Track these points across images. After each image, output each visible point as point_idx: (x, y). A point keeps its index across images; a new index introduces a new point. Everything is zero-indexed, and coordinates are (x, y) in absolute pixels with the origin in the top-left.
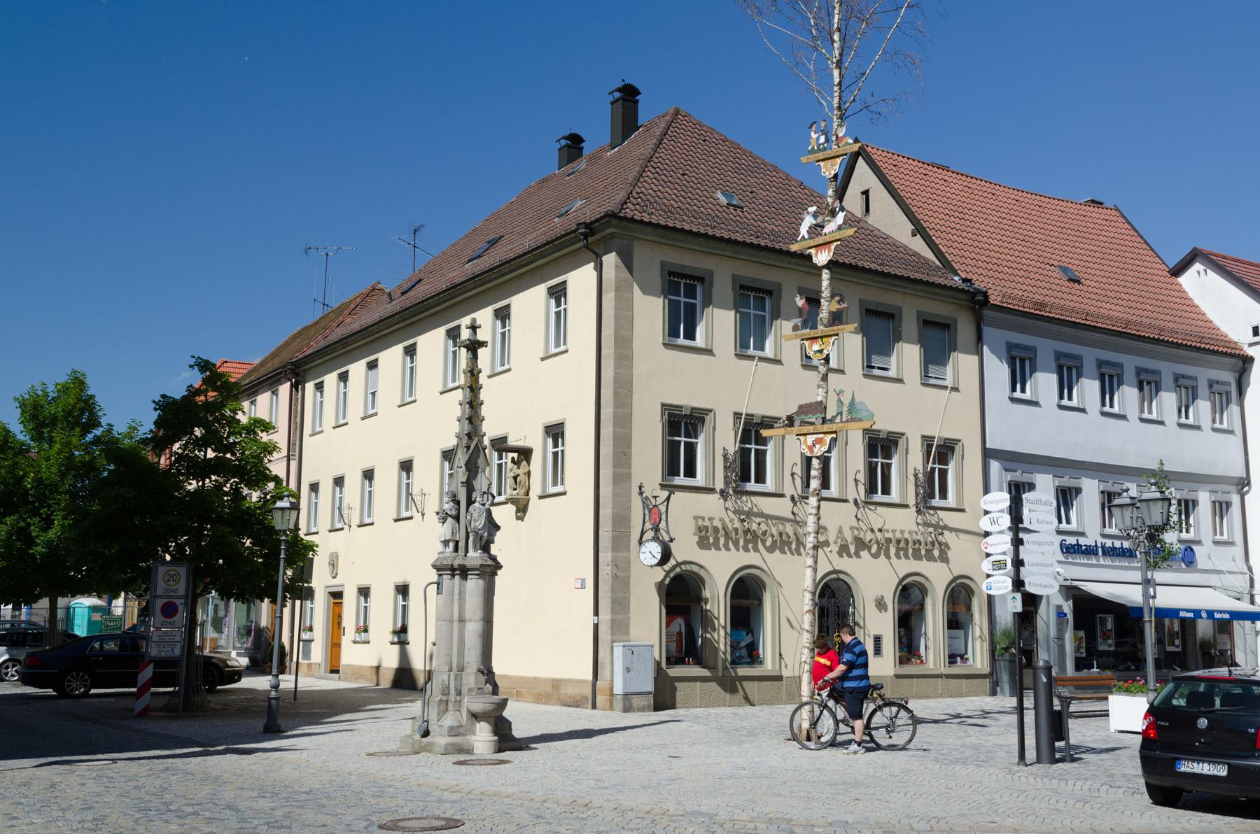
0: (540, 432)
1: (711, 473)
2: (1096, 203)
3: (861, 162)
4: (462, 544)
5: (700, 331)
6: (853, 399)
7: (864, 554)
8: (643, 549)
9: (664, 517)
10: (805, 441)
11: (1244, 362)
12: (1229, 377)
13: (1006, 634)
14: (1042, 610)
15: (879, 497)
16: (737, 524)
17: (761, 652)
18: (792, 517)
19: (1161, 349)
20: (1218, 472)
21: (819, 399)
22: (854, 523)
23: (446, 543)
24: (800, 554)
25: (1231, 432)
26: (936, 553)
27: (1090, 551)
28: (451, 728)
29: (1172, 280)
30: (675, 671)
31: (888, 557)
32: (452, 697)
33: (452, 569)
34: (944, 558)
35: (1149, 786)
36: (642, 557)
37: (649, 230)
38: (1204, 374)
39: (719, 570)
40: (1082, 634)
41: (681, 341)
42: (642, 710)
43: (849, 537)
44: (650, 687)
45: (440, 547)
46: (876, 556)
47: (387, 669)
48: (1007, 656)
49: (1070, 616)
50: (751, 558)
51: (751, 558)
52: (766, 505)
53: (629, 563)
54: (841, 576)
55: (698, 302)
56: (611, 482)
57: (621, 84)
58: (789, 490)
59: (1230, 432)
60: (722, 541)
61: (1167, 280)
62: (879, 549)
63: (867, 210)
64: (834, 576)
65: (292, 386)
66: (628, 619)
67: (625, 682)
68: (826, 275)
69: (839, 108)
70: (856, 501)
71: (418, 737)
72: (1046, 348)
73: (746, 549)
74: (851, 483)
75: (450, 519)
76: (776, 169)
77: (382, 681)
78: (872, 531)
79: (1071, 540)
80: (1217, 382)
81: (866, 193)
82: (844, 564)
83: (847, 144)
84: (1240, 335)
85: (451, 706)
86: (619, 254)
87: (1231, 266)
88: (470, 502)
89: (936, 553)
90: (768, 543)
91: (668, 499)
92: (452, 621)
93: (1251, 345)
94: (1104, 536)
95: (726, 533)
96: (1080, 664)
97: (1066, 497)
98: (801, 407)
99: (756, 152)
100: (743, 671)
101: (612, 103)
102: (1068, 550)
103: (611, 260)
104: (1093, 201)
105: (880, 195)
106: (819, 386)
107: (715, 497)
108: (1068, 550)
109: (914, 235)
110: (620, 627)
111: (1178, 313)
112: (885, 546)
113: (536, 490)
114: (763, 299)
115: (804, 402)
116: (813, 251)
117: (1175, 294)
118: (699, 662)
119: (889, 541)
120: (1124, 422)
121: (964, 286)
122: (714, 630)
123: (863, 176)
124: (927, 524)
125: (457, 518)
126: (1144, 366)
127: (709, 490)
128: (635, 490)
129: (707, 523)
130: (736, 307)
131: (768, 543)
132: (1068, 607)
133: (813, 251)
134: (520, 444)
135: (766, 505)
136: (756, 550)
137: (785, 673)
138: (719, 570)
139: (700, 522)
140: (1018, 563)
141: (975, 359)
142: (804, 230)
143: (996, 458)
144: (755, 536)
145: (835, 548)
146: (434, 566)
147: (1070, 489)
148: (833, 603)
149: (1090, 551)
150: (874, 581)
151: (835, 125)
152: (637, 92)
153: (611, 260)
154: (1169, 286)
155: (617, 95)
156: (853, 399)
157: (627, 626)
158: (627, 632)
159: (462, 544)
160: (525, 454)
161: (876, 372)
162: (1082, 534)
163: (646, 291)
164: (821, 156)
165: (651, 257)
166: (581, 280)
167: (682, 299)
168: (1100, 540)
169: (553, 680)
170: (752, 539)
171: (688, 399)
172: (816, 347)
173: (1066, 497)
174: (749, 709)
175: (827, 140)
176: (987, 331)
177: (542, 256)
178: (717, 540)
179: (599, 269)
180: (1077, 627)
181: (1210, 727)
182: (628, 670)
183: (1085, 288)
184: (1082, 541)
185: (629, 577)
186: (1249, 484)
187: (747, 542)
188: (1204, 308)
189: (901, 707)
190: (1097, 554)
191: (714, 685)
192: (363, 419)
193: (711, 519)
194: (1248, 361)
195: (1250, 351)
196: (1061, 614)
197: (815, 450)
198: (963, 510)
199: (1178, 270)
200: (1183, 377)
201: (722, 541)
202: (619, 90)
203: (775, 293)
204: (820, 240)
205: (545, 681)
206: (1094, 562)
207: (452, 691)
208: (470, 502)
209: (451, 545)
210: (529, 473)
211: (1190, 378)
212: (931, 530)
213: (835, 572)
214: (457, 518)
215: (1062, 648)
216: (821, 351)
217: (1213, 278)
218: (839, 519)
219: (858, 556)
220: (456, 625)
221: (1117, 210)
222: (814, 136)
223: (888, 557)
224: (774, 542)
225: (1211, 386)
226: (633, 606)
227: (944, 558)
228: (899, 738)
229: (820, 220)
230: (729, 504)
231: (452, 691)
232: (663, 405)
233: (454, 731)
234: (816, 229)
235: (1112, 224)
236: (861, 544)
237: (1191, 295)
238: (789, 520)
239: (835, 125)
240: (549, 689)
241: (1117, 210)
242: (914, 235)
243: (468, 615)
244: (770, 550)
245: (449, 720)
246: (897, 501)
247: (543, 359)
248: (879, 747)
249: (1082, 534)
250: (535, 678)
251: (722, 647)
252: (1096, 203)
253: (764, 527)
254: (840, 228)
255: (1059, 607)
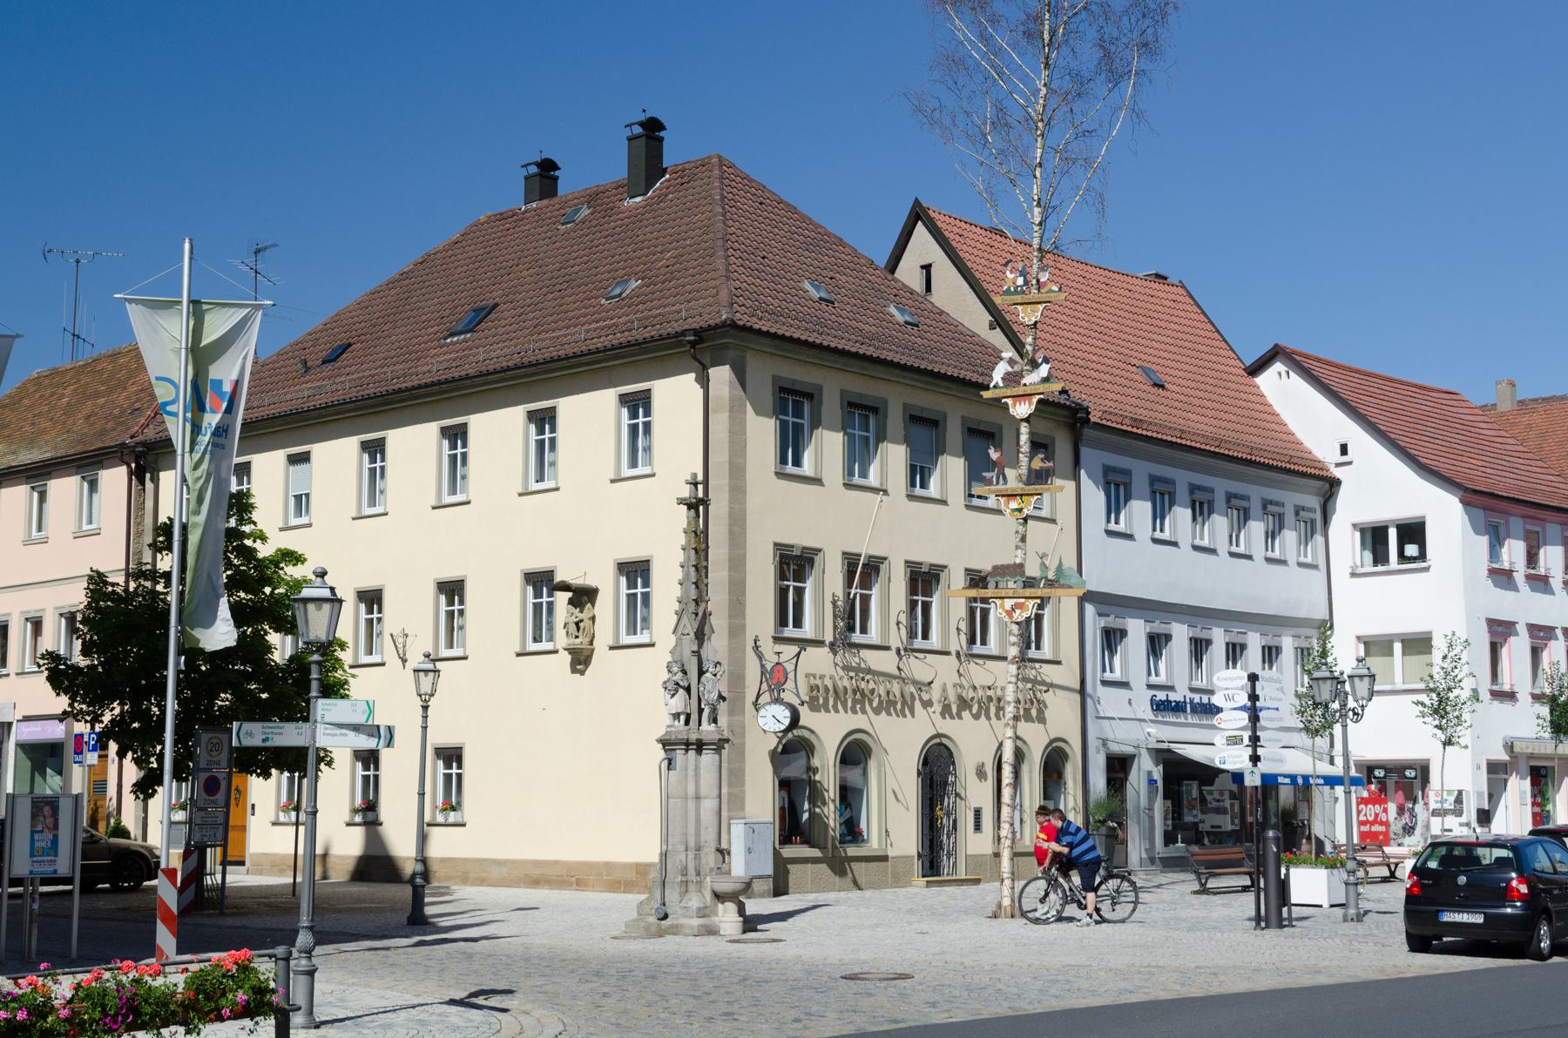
0: (610, 570)
1: (820, 624)
2: (1160, 277)
3: (920, 228)
4: (694, 717)
5: (807, 457)
6: (1060, 564)
7: (966, 714)
8: (762, 712)
9: (791, 676)
10: (1002, 606)
11: (1332, 486)
12: (1313, 502)
13: (1099, 805)
14: (1133, 776)
15: (919, 643)
16: (846, 683)
17: (863, 825)
18: (896, 672)
19: (1251, 470)
20: (1302, 613)
21: (1018, 561)
22: (956, 680)
23: (676, 716)
24: (837, 711)
25: (1315, 567)
26: (1034, 713)
27: (1178, 708)
28: (699, 909)
29: (1249, 380)
30: (788, 852)
31: (988, 718)
32: (692, 876)
33: (687, 744)
34: (1042, 719)
35: (1409, 935)
36: (761, 721)
37: (765, 340)
38: (1291, 498)
39: (829, 731)
40: (1169, 803)
41: (790, 469)
42: (762, 896)
43: (952, 698)
44: (769, 871)
45: (668, 720)
46: (976, 717)
47: (341, 857)
48: (1103, 830)
49: (1160, 784)
50: (859, 721)
51: (859, 721)
52: (874, 659)
53: (743, 728)
54: (945, 741)
55: (806, 422)
56: (726, 635)
57: (642, 117)
58: (895, 642)
59: (1314, 567)
60: (831, 702)
61: (1239, 379)
62: (980, 707)
63: (928, 288)
64: (937, 740)
65: (130, 473)
66: (743, 792)
67: (747, 864)
68: (1024, 429)
69: (1040, 249)
70: (958, 654)
71: (652, 920)
72: (1141, 470)
73: (854, 712)
74: (953, 632)
75: (681, 691)
76: (841, 242)
77: (332, 873)
78: (975, 688)
79: (1161, 696)
80: (1303, 509)
81: (927, 268)
82: (947, 726)
83: (1051, 291)
84: (1326, 453)
85: (692, 887)
86: (732, 368)
87: (1319, 371)
88: (701, 673)
89: (1034, 713)
90: (875, 704)
91: (798, 655)
92: (686, 798)
93: (1338, 465)
94: (1192, 690)
95: (835, 691)
96: (1169, 839)
97: (1156, 643)
98: (995, 568)
99: (816, 219)
100: (852, 851)
101: (630, 139)
102: (1160, 707)
103: (721, 375)
104: (1158, 276)
105: (945, 272)
106: (1017, 548)
107: (824, 652)
108: (1160, 707)
109: (992, 328)
110: (738, 802)
111: (1247, 413)
112: (986, 705)
113: (604, 634)
114: (867, 418)
115: (999, 563)
116: (1010, 401)
117: (1253, 398)
118: (808, 842)
119: (990, 699)
120: (1212, 557)
121: (1062, 399)
122: (824, 803)
123: (922, 245)
124: (1026, 680)
125: (688, 690)
126: (1233, 491)
127: (819, 643)
128: (750, 644)
129: (818, 682)
130: (844, 429)
131: (875, 704)
132: (1158, 773)
133: (1010, 401)
134: (576, 580)
135: (874, 659)
136: (864, 712)
137: (891, 853)
138: (829, 731)
139: (812, 681)
140: (1255, 740)
141: (1072, 484)
142: (998, 376)
143: (1091, 601)
144: (863, 694)
145: (937, 708)
146: (660, 741)
147: (1114, 630)
148: (936, 769)
149: (1178, 708)
150: (973, 742)
151: (1035, 267)
152: (662, 127)
153: (721, 375)
154: (1247, 389)
155: (638, 130)
156: (1060, 564)
157: (743, 800)
158: (742, 808)
159: (694, 717)
160: (583, 596)
161: (976, 502)
162: (1171, 688)
163: (759, 412)
164: (1019, 299)
165: (765, 370)
166: (676, 397)
167: (791, 419)
168: (1190, 695)
169: (637, 864)
170: (861, 699)
171: (800, 539)
172: (1014, 505)
173: (1156, 643)
174: (856, 894)
175: (1026, 283)
176: (1084, 451)
177: (616, 357)
178: (826, 700)
179: (704, 381)
180: (1165, 798)
181: (1467, 884)
182: (749, 851)
183: (1167, 394)
184: (1173, 697)
185: (744, 744)
186: (1331, 627)
187: (855, 702)
188: (1286, 416)
189: (1123, 878)
190: (1184, 711)
191: (824, 866)
192: (281, 530)
193: (822, 677)
194: (1334, 483)
195: (1337, 473)
196: (1152, 782)
197: (1015, 615)
198: (1059, 663)
199: (1256, 369)
200: (1271, 502)
201: (831, 702)
202: (641, 124)
203: (881, 411)
204: (1020, 390)
205: (626, 866)
206: (1182, 720)
207: (692, 871)
208: (701, 673)
209: (682, 718)
210: (593, 619)
211: (1277, 504)
212: (1029, 686)
213: (939, 735)
214: (688, 690)
215: (1152, 819)
216: (1020, 510)
217: (1297, 382)
218: (941, 673)
219: (960, 718)
220: (691, 804)
221: (1183, 287)
222: (1010, 276)
223: (988, 718)
224: (881, 702)
225: (1297, 514)
226: (748, 778)
227: (1042, 719)
228: (1123, 910)
229: (1017, 368)
230: (838, 659)
231: (692, 871)
232: (776, 544)
233: (703, 913)
234: (1012, 379)
235: (1181, 306)
236: (964, 704)
237: (1270, 400)
238: (895, 677)
239: (1035, 267)
240: (631, 875)
241: (1183, 287)
242: (992, 328)
243: (703, 792)
244: (877, 711)
245: (694, 902)
246: (995, 652)
247: (613, 481)
248: (1104, 920)
249: (1171, 688)
250: (607, 864)
251: (832, 823)
252: (1160, 277)
253: (872, 685)
254: (1046, 380)
255: (1150, 773)
